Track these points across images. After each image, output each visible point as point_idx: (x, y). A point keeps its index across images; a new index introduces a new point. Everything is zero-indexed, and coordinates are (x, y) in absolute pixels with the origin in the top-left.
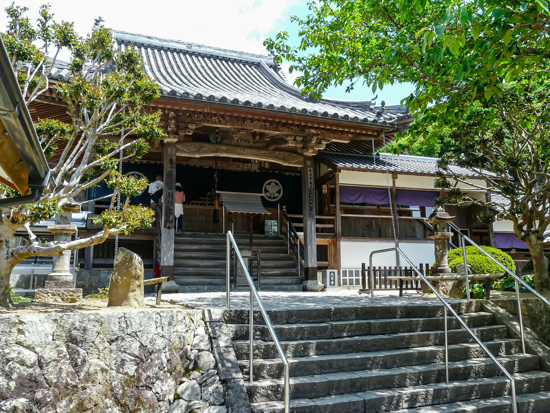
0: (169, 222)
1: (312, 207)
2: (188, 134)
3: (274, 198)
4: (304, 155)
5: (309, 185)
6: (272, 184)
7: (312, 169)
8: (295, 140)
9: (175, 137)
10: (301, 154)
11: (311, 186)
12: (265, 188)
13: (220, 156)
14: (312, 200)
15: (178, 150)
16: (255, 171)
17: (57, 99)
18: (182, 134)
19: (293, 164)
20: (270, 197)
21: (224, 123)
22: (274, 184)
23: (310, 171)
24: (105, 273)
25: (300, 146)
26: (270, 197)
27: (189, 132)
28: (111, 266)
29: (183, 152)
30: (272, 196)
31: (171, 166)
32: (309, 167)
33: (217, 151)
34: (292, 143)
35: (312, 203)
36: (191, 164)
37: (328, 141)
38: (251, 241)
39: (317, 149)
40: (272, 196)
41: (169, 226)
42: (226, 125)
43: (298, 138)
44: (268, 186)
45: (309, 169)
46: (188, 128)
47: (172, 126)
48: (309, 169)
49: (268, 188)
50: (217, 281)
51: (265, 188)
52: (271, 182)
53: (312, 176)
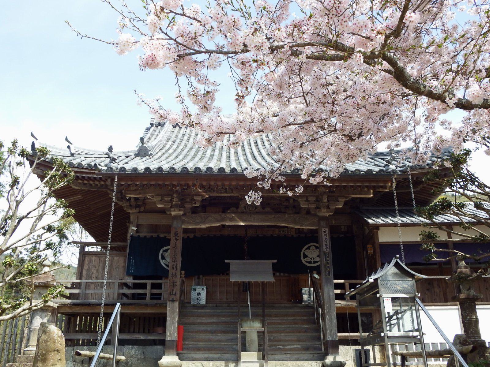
0: (173, 294)
1: (329, 272)
2: (194, 205)
3: (315, 262)
4: (318, 216)
5: (324, 247)
6: (311, 248)
7: (327, 229)
8: (307, 200)
9: (180, 210)
10: (315, 215)
11: (327, 249)
12: (304, 253)
13: (227, 224)
14: (328, 264)
15: (183, 222)
16: (292, 236)
17: (93, 185)
18: (188, 206)
19: (306, 226)
20: (310, 262)
21: (230, 191)
22: (314, 248)
23: (325, 232)
24: (129, 348)
25: (313, 206)
26: (310, 262)
27: (195, 204)
28: (162, 342)
29: (189, 223)
30: (312, 261)
31: (176, 239)
32: (324, 227)
33: (223, 220)
34: (304, 204)
35: (329, 267)
36: (225, 233)
37: (346, 197)
38: (264, 312)
39: (334, 207)
40: (312, 261)
41: (173, 299)
42: (232, 193)
43: (310, 199)
44: (307, 250)
45: (323, 230)
46: (195, 200)
47: (175, 200)
48: (323, 230)
49: (307, 252)
50: (363, 356)
51: (304, 253)
52: (310, 246)
53: (327, 238)
